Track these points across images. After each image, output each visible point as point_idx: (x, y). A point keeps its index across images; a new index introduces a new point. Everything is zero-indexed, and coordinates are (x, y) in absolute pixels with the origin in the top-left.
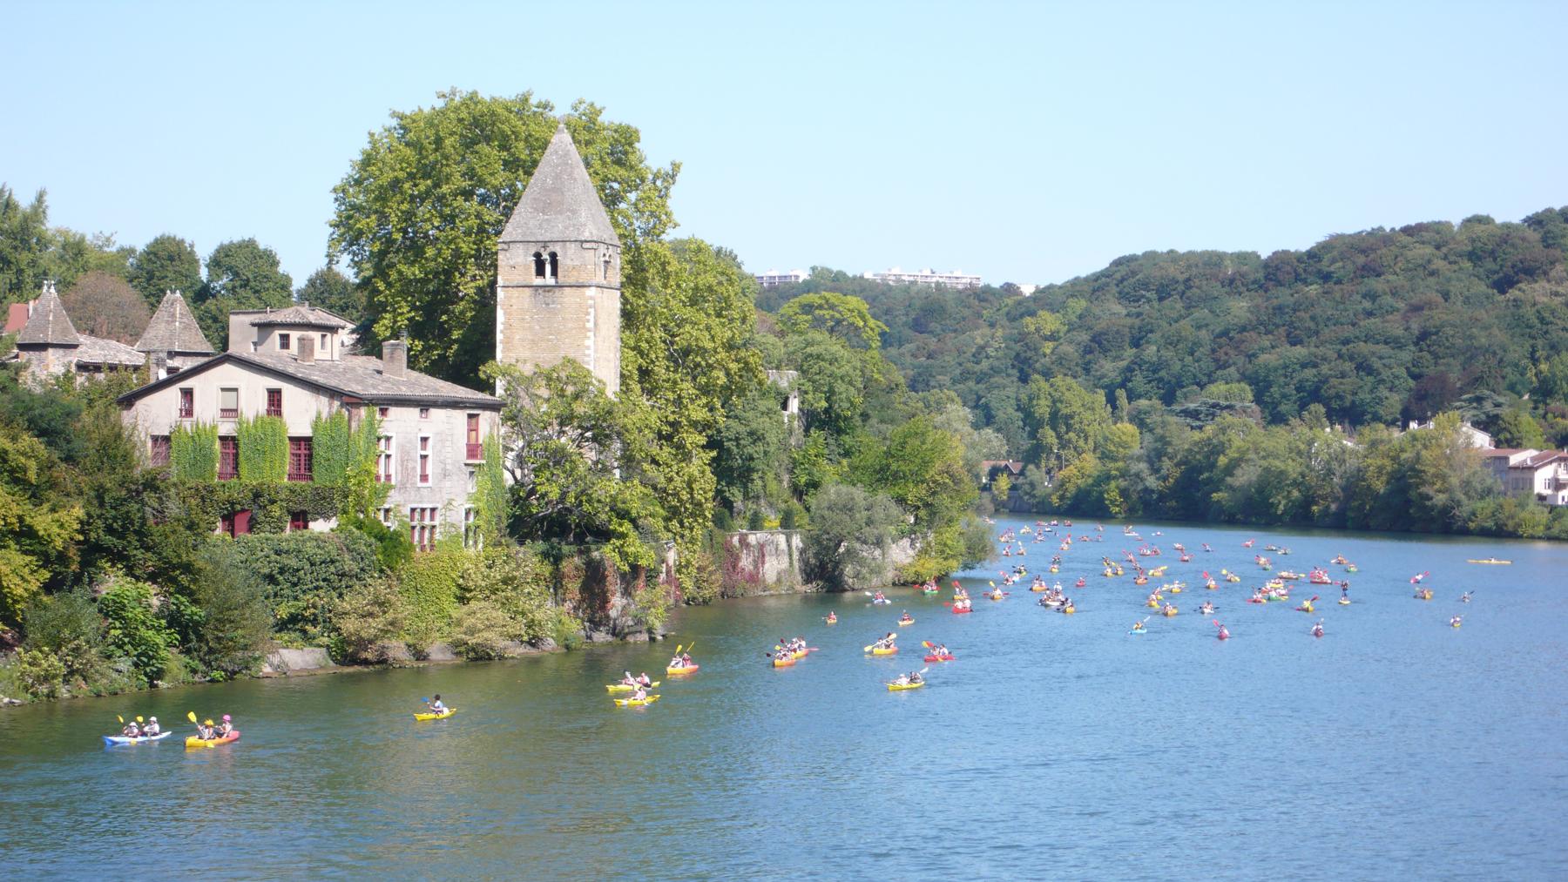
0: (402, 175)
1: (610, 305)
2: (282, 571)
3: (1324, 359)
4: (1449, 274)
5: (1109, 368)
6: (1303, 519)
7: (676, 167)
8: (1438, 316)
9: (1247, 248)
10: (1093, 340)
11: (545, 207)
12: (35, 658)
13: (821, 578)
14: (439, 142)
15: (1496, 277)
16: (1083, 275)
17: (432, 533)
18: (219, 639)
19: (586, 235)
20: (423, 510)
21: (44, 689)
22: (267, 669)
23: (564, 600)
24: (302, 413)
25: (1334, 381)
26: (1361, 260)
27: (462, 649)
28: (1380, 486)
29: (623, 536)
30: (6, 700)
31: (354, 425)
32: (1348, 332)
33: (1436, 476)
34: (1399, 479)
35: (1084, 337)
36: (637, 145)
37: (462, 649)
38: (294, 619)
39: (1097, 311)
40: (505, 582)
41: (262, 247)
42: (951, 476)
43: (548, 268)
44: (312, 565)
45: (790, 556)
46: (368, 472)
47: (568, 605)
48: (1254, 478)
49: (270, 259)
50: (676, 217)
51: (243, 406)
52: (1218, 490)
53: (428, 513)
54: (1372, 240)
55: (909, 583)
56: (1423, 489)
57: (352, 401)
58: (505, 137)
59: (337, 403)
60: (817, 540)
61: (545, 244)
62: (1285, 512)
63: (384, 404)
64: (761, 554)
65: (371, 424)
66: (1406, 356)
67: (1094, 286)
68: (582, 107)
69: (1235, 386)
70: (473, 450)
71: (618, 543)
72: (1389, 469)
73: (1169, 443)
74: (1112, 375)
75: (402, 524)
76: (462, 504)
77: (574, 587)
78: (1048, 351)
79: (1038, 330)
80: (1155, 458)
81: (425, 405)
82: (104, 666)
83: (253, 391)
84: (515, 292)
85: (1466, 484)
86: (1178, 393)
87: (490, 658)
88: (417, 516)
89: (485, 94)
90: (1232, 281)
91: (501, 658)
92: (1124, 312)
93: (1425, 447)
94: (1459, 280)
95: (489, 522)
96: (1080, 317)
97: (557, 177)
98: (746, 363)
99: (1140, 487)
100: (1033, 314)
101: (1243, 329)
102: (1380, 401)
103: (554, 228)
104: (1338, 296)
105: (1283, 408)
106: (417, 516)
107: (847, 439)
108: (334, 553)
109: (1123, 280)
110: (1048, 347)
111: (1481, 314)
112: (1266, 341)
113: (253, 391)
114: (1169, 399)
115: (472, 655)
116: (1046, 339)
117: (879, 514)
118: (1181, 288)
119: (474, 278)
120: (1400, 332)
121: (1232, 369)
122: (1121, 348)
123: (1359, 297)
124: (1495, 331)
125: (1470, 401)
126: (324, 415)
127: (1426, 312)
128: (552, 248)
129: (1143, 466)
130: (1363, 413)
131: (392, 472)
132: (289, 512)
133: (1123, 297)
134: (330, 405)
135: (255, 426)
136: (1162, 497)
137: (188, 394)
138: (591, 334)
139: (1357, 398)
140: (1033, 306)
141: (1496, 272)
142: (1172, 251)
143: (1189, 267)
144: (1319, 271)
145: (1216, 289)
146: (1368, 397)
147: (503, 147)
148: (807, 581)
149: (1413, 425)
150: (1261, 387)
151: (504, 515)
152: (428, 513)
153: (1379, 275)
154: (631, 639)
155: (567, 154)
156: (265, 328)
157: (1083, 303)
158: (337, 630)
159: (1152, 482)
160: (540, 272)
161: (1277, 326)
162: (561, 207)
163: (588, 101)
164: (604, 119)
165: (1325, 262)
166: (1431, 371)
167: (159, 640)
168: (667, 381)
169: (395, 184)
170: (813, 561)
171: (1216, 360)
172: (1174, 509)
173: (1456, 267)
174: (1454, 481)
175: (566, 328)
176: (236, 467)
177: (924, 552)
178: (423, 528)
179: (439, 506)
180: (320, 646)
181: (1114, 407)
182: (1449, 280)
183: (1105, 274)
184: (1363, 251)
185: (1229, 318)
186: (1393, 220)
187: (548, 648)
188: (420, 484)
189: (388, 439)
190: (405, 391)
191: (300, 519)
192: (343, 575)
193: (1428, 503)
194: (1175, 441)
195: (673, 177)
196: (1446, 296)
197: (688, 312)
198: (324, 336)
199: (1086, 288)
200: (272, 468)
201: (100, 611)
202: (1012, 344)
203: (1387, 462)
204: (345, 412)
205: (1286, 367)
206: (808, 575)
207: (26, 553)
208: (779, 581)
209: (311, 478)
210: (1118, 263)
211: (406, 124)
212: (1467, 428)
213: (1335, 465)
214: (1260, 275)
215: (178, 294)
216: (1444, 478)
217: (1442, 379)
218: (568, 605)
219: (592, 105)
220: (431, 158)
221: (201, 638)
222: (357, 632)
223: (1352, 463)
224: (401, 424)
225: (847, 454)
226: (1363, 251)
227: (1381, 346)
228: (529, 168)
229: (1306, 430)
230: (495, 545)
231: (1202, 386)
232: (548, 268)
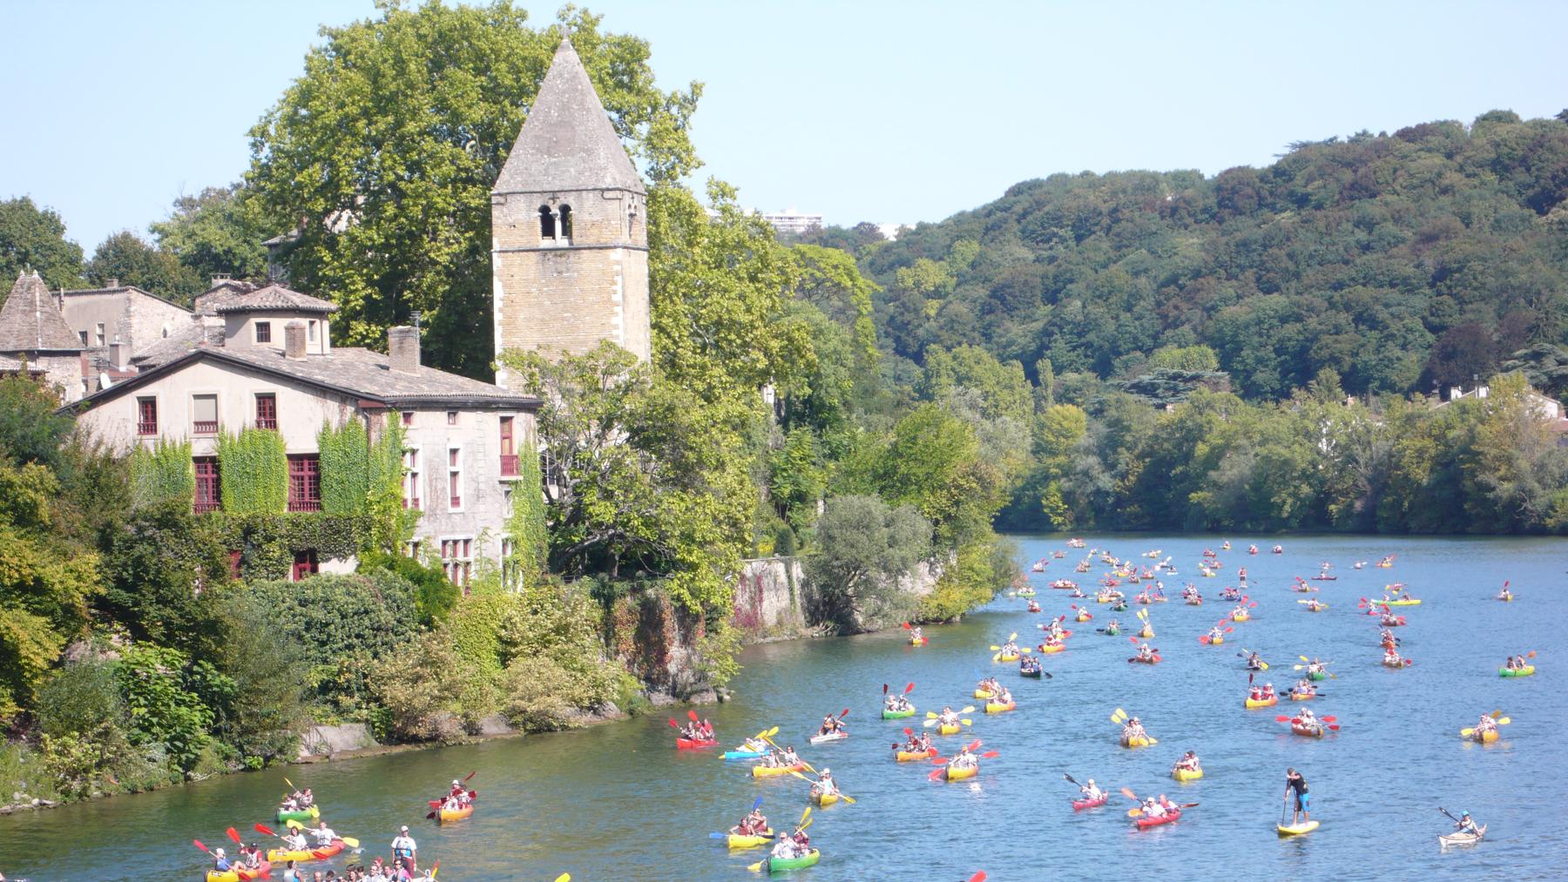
0: (353, 110)
1: (637, 267)
2: (309, 626)
3: (1311, 309)
4: (1468, 191)
5: (1018, 332)
6: (1315, 520)
7: (696, 89)
8: (1461, 246)
9: (1186, 165)
10: (993, 295)
11: (549, 148)
12: (64, 745)
13: (830, 618)
14: (400, 64)
15: (1531, 192)
16: (969, 208)
17: (466, 572)
18: (250, 715)
19: (608, 182)
20: (455, 542)
21: (76, 786)
22: (304, 754)
23: (617, 653)
24: (304, 424)
25: (1326, 339)
26: (1347, 176)
27: (519, 719)
28: (1422, 475)
29: (693, 567)
30: (36, 801)
31: (374, 436)
32: (1343, 273)
33: (1497, 458)
34: (1446, 465)
35: (982, 292)
36: (646, 62)
37: (519, 719)
38: (325, 688)
39: (994, 256)
40: (557, 631)
41: (40, 209)
42: (980, 479)
43: (558, 225)
44: (343, 617)
45: (791, 589)
46: (394, 497)
47: (622, 659)
48: (1247, 472)
49: (52, 223)
50: (699, 154)
51: (224, 417)
52: (1198, 489)
53: (461, 546)
54: (1359, 149)
55: (938, 621)
56: (1481, 477)
57: (370, 405)
58: (480, 56)
59: (350, 409)
60: (825, 568)
61: (554, 195)
62: (1291, 515)
63: (409, 407)
64: (758, 587)
65: (395, 434)
66: (1420, 301)
67: (988, 223)
68: (572, 14)
69: (1194, 351)
70: (508, 463)
71: (687, 576)
72: (1433, 452)
73: (1128, 429)
74: (1022, 341)
75: (434, 560)
76: (499, 533)
77: (627, 634)
78: (932, 313)
79: (917, 284)
80: (1107, 449)
81: (452, 407)
82: (133, 754)
83: (237, 399)
84: (517, 258)
85: (1541, 467)
86: (1117, 362)
87: (550, 729)
88: (449, 550)
90: (1174, 211)
91: (564, 728)
92: (1031, 257)
93: (1482, 421)
94: (1482, 198)
95: (529, 555)
96: (973, 265)
97: (565, 107)
98: (790, 340)
99: (1090, 488)
100: (907, 263)
101: (1197, 274)
102: (1390, 363)
103: (565, 174)
104: (1321, 225)
105: (1260, 377)
106: (449, 550)
107: (834, 437)
108: (369, 600)
109: (1024, 215)
110: (932, 307)
111: (1515, 241)
112: (1229, 289)
113: (237, 399)
114: (1104, 369)
115: (530, 726)
116: (929, 296)
117: (904, 531)
118: (1106, 221)
119: (447, 242)
120: (1410, 270)
121: (1187, 327)
122: (1031, 304)
123: (1350, 226)
124: (1538, 265)
125: (1526, 358)
126: (334, 425)
127: (1442, 242)
128: (562, 200)
129: (1093, 460)
130: (1367, 381)
131: (420, 495)
132: (292, 551)
133: (1027, 236)
134: (342, 412)
135: (242, 443)
136: (1120, 501)
137: (149, 405)
138: (618, 309)
139: (1359, 361)
140: (906, 253)
141: (1531, 186)
142: (1086, 174)
143: (1114, 194)
144: (1292, 194)
145: (1154, 222)
146: (1373, 359)
147: (478, 72)
148: (813, 620)
149: (1456, 393)
150: (1228, 351)
151: (545, 546)
152: (461, 546)
153: (1373, 196)
154: (696, 700)
155: (575, 77)
156: (235, 315)
157: (976, 247)
158: (378, 700)
159: (1106, 481)
160: (548, 230)
161: (1242, 268)
162: (566, 147)
163: (580, 6)
164: (600, 31)
165: (1299, 179)
166: (1455, 320)
167: (197, 717)
168: (693, 366)
169: (347, 124)
170: (817, 596)
171: (1164, 317)
172: (1137, 516)
173: (1476, 182)
174: (1524, 464)
175: (581, 305)
176: (218, 495)
177: (946, 580)
178: (456, 566)
179: (473, 536)
180: (358, 721)
181: (1036, 383)
182: (1468, 199)
183: (1001, 207)
184: (1349, 165)
185: (1177, 259)
186: (1386, 121)
187: (612, 715)
188: (451, 510)
189: (414, 452)
190: (427, 391)
191: (307, 559)
192: (379, 629)
193: (1491, 495)
194: (1135, 426)
195: (693, 102)
196: (1467, 220)
197: (714, 277)
198: (312, 323)
199: (975, 226)
200: (266, 496)
201: (121, 688)
202: (881, 304)
203: (1428, 442)
204: (361, 420)
205: (1260, 322)
206: (812, 614)
207: (36, 612)
208: (780, 623)
209: (320, 507)
210: (1017, 191)
211: (342, 48)
212: (1534, 397)
213: (1357, 449)
214: (1212, 201)
215: (36, 274)
216: (1509, 460)
217: (1472, 332)
218: (622, 659)
219: (585, 12)
220: (393, 87)
221: (232, 715)
222: (409, 702)
223: (1380, 446)
224: (427, 430)
225: (833, 455)
226: (1349, 165)
227: (1386, 290)
228: (520, 95)
229: (1313, 404)
230: (537, 585)
231: (1148, 352)
232: (558, 225)
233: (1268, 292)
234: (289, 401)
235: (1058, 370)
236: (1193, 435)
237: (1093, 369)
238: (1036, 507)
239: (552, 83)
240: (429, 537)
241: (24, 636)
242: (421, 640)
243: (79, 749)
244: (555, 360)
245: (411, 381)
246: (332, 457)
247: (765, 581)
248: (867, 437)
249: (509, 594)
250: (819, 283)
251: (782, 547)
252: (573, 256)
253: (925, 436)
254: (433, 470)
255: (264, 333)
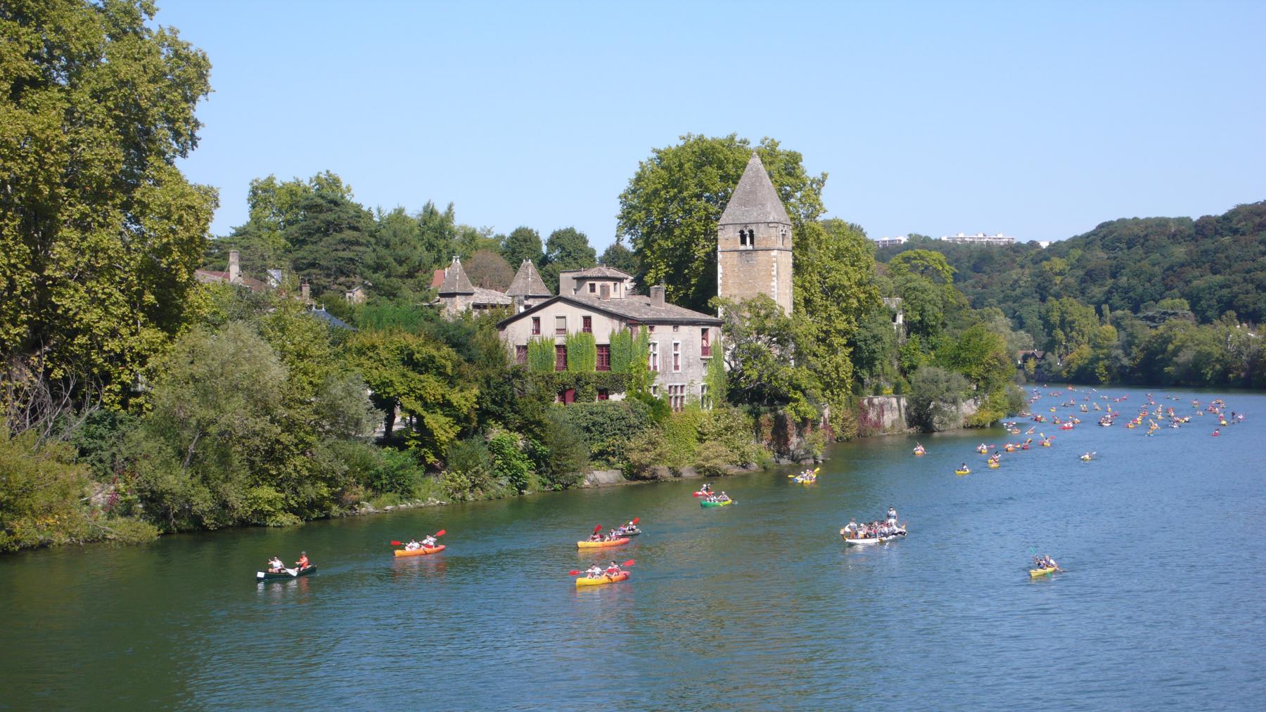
0: (659, 186)
1: (787, 259)
2: (594, 425)
3: (1235, 282)
5: (1097, 291)
7: (825, 176)
10: (1086, 274)
11: (745, 203)
14: (681, 166)
19: (771, 219)
21: (459, 495)
22: (587, 483)
24: (603, 331)
25: (1241, 296)
26: (1258, 220)
29: (797, 400)
32: (1250, 265)
35: (1081, 273)
39: (1089, 256)
40: (726, 429)
43: (748, 240)
46: (643, 365)
49: (583, 239)
57: (632, 322)
59: (624, 324)
60: (916, 401)
61: (746, 225)
63: (652, 323)
65: (644, 336)
67: (1086, 241)
69: (1177, 300)
75: (664, 395)
77: (767, 432)
80: (1127, 346)
81: (676, 324)
82: (492, 482)
84: (729, 255)
89: (708, 137)
90: (1174, 236)
91: (725, 474)
96: (1078, 260)
97: (753, 184)
100: (1047, 259)
101: (1182, 265)
103: (753, 215)
104: (1243, 243)
105: (1209, 314)
107: (933, 339)
110: (1058, 279)
112: (1197, 273)
113: (575, 317)
114: (1135, 310)
116: (1057, 274)
117: (954, 385)
118: (1142, 241)
119: (703, 247)
122: (1104, 279)
128: (750, 227)
129: (1120, 351)
133: (1104, 247)
136: (1133, 370)
137: (537, 320)
145: (1164, 241)
148: (910, 426)
150: (1194, 300)
154: (803, 463)
155: (758, 170)
156: (581, 280)
157: (1080, 252)
159: (1126, 361)
160: (743, 242)
162: (756, 203)
164: (780, 148)
169: (656, 192)
171: (1166, 285)
175: (759, 276)
176: (566, 363)
177: (982, 407)
183: (1093, 233)
184: (1259, 215)
189: (655, 344)
190: (664, 316)
191: (604, 393)
197: (834, 264)
205: (1210, 288)
208: (893, 426)
210: (1101, 226)
211: (661, 156)
213: (1243, 348)
214: (1193, 231)
218: (765, 443)
221: (547, 465)
224: (662, 335)
225: (934, 348)
226: (1259, 215)
232: (748, 240)
233: (1215, 274)
234: (598, 321)
235: (1112, 309)
236: (1168, 340)
237: (1130, 309)
238: (1093, 373)
239: (747, 175)
240: (662, 383)
241: (436, 426)
242: (651, 433)
243: (464, 479)
244: (737, 301)
245: (659, 311)
246: (616, 345)
247: (885, 407)
248: (947, 340)
249: (706, 411)
250: (926, 268)
251: (897, 391)
252: (754, 254)
253: (975, 340)
254: (664, 352)
255: (593, 288)
